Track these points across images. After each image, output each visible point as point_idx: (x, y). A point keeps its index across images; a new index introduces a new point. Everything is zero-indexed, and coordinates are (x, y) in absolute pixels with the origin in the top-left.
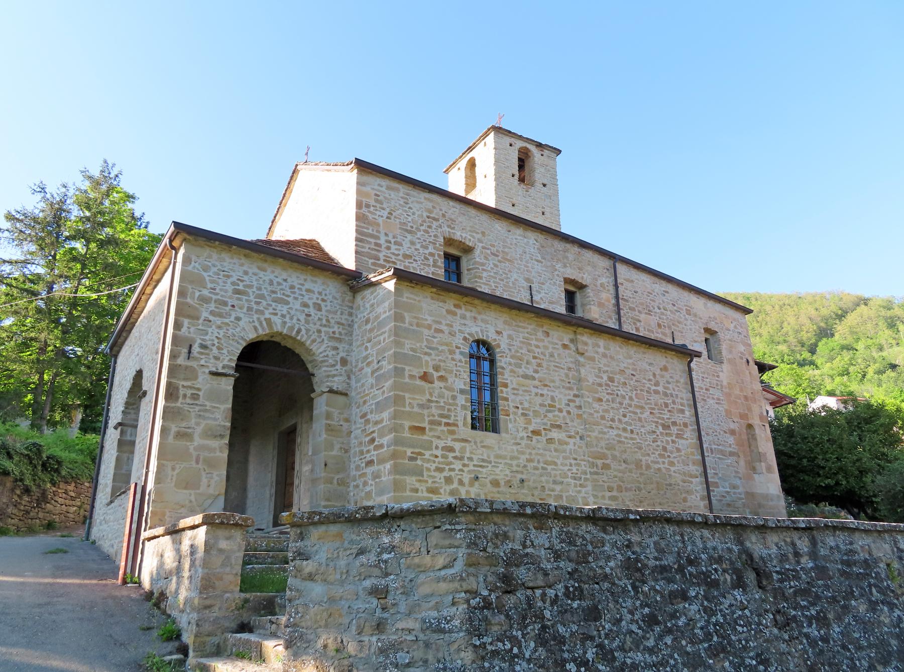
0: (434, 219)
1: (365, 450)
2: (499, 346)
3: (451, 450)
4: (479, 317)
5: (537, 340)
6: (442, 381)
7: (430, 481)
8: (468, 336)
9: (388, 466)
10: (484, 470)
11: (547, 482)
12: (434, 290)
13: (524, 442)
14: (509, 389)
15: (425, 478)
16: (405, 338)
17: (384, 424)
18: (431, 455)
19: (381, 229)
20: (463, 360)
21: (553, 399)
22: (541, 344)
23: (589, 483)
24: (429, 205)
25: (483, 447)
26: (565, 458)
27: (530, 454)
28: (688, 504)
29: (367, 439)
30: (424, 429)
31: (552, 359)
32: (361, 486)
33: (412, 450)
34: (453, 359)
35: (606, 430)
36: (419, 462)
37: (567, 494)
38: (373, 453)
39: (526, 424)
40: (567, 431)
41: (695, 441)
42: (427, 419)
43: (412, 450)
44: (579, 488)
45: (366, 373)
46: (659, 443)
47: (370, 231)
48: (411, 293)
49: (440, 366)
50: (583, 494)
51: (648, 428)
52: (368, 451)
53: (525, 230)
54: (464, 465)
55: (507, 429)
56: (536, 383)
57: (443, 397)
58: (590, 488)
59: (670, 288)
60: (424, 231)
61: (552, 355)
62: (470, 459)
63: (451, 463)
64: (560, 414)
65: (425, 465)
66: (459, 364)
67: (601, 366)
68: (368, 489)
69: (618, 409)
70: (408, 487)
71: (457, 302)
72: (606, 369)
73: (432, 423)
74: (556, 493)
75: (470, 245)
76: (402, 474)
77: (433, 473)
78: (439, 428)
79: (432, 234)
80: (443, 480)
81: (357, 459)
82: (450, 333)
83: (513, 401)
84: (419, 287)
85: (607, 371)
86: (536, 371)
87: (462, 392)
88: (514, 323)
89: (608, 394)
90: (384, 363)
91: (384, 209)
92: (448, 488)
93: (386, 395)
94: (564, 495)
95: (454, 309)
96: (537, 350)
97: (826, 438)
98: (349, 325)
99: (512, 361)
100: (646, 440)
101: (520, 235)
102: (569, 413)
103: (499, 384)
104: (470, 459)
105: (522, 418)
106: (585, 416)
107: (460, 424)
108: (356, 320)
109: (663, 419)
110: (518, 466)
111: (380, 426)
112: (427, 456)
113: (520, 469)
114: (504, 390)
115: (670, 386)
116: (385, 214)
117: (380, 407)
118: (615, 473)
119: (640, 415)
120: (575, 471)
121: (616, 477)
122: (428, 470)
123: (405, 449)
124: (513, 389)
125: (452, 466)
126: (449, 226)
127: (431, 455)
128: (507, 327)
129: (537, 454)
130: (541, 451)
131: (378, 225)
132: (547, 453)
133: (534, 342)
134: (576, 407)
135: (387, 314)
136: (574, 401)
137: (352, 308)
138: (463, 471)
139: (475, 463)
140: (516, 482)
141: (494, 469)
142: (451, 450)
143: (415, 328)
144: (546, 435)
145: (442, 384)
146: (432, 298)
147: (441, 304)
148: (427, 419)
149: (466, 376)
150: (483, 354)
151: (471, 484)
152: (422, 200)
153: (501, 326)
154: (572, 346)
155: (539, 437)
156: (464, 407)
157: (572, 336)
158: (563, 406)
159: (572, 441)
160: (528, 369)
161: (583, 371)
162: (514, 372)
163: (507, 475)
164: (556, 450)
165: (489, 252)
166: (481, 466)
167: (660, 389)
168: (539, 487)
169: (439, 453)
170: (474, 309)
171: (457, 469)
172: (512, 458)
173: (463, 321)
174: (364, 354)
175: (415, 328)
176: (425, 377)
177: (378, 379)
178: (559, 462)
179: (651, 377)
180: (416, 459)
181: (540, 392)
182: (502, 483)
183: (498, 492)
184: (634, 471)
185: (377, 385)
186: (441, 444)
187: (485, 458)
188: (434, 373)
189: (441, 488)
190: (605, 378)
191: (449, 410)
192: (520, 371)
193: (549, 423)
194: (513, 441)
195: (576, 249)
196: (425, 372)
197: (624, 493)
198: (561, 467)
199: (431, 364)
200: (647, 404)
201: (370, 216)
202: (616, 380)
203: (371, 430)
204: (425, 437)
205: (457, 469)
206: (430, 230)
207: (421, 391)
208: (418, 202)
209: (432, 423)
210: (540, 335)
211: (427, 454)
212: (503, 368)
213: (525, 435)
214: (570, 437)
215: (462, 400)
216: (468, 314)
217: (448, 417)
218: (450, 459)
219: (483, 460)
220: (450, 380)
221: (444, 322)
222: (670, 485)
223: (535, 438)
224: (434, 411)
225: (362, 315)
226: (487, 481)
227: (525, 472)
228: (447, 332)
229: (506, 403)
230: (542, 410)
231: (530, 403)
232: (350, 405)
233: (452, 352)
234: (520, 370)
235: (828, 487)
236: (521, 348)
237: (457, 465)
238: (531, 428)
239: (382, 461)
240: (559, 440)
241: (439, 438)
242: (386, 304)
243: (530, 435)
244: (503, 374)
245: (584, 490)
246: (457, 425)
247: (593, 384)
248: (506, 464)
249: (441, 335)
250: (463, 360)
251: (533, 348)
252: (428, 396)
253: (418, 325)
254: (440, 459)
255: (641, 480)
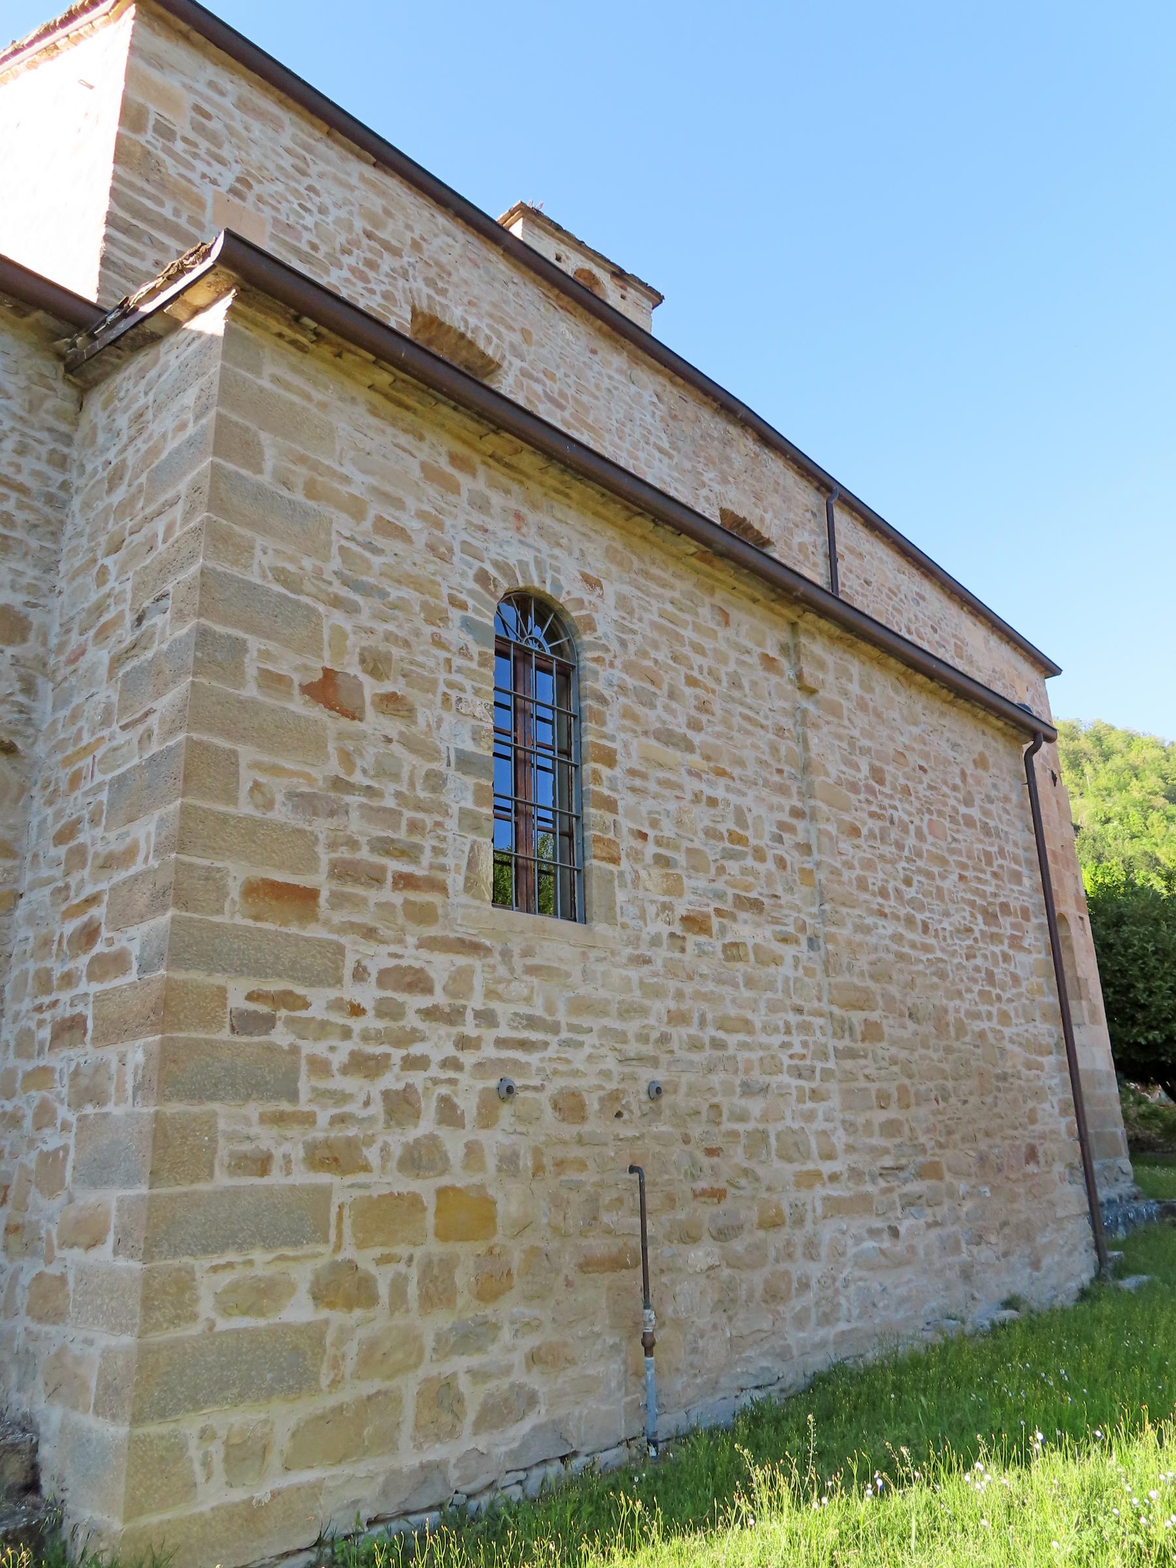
0: (387, 246)
1: (57, 974)
2: (591, 626)
3: (418, 982)
4: (532, 517)
5: (697, 628)
6: (395, 713)
7: (323, 1117)
8: (493, 572)
9: (137, 1053)
10: (533, 1059)
11: (728, 1089)
12: (384, 378)
13: (661, 955)
14: (617, 772)
15: (304, 1106)
16: (252, 525)
17: (138, 867)
18: (337, 1005)
19: (208, 216)
20: (475, 649)
21: (740, 819)
22: (708, 644)
23: (833, 1086)
24: (377, 204)
25: (531, 970)
26: (773, 1008)
27: (680, 995)
28: (1039, 1127)
29: (71, 927)
30: (311, 895)
31: (736, 694)
32: (28, 1123)
33: (254, 984)
34: (438, 642)
35: (869, 921)
36: (281, 1037)
37: (780, 1126)
38: (84, 987)
39: (667, 892)
40: (776, 921)
41: (1042, 956)
42: (325, 857)
43: (254, 984)
44: (809, 1105)
45: (93, 669)
46: (979, 961)
47: (167, 212)
48: (295, 369)
49: (388, 658)
50: (819, 1124)
51: (956, 918)
52: (68, 980)
53: (635, 360)
54: (463, 1043)
55: (611, 908)
56: (695, 760)
57: (396, 777)
58: (835, 1102)
59: (928, 589)
60: (353, 270)
61: (736, 684)
62: (486, 1018)
63: (414, 1037)
64: (758, 866)
65: (308, 1048)
66: (458, 661)
67: (856, 733)
68: (52, 1140)
69: (893, 862)
70: (224, 1149)
71: (461, 449)
72: (865, 743)
73: (343, 871)
74: (750, 1126)
75: (490, 352)
76: (197, 1093)
77: (339, 1082)
78: (374, 896)
79: (378, 288)
80: (377, 1108)
81: (27, 1004)
82: (432, 548)
83: (632, 813)
84: (326, 351)
85: (869, 750)
86: (696, 726)
87: (465, 762)
88: (637, 564)
89: (872, 815)
90: (157, 620)
91: (222, 161)
92: (398, 1140)
93: (155, 748)
94: (773, 1129)
95: (449, 469)
96: (697, 660)
97: (1151, 947)
98: (50, 499)
99: (630, 682)
100: (954, 954)
101: (620, 371)
102: (781, 863)
103: (587, 751)
104: (486, 1018)
105: (656, 872)
106: (822, 876)
107: (455, 881)
108: (78, 482)
109: (983, 895)
110: (643, 1038)
111: (121, 875)
112: (317, 1011)
113: (648, 1050)
114: (605, 771)
115: (992, 807)
116: (228, 179)
117: (129, 797)
118: (893, 1050)
119: (938, 882)
120: (797, 1049)
121: (894, 1061)
122: (320, 1067)
123: (218, 979)
124: (632, 772)
125: (417, 1049)
126: (430, 282)
127: (337, 1005)
128: (614, 569)
129: (698, 995)
130: (711, 986)
131: (201, 205)
132: (726, 990)
133: (688, 633)
134: (798, 846)
135: (191, 430)
136: (792, 829)
137: (68, 440)
138: (456, 1065)
139: (504, 1032)
140: (636, 1097)
141: (569, 1053)
142: (418, 982)
143: (299, 496)
144: (723, 930)
145: (393, 727)
146: (374, 411)
147: (404, 440)
148: (325, 857)
149: (480, 708)
150: (536, 639)
151: (487, 1119)
152: (354, 181)
153: (598, 565)
154: (784, 663)
155: (703, 939)
156: (469, 820)
157: (785, 636)
158: (765, 842)
159: (788, 951)
160: (673, 712)
161: (813, 741)
162: (635, 718)
163: (606, 1074)
164: (750, 983)
165: (539, 388)
166: (524, 1045)
167: (975, 812)
168: (704, 1108)
169: (367, 995)
170: (515, 487)
171: (436, 1057)
172: (627, 1011)
173: (477, 518)
174: (94, 597)
175: (299, 496)
176: (326, 689)
177: (129, 686)
178: (758, 1020)
179: (958, 781)
180: (268, 1022)
181: (708, 791)
182: (593, 1104)
183: (580, 1141)
184: (932, 1041)
185: (124, 710)
186: (378, 958)
187: (539, 1011)
188: (365, 679)
189: (370, 1141)
190: (865, 770)
191: (414, 827)
192: (653, 717)
193: (730, 892)
194: (629, 950)
195: (747, 444)
196: (328, 674)
197: (913, 1109)
198: (764, 1039)
199: (354, 642)
200: (952, 851)
201: (171, 168)
202: (888, 778)
203: (89, 890)
204: (314, 931)
205: (436, 1057)
206: (371, 274)
207: (310, 742)
208: (336, 179)
209: (343, 871)
210: (705, 612)
211: (319, 1000)
212: (602, 700)
213: (665, 930)
214: (785, 939)
215: (465, 794)
216: (497, 499)
217: (409, 853)
218: (412, 1021)
219: (532, 1022)
220: (424, 716)
221: (411, 503)
222: (1004, 1077)
223: (692, 939)
224: (356, 825)
225: (99, 461)
226: (544, 1098)
227: (665, 1058)
228: (421, 540)
229: (609, 817)
230: (713, 851)
231: (679, 823)
232: (23, 790)
233: (435, 616)
234: (652, 714)
235: (1152, 1046)
236: (655, 645)
237: (437, 1044)
238: (681, 910)
239: (115, 1030)
240: (757, 947)
241: (370, 933)
242: (189, 398)
243: (678, 929)
244: (601, 720)
245: (821, 1108)
246: (442, 888)
247: (839, 783)
248: (606, 1032)
249: (398, 546)
250: (475, 649)
251: (687, 650)
252: (334, 767)
253: (311, 490)
254: (370, 1021)
255: (946, 1067)
